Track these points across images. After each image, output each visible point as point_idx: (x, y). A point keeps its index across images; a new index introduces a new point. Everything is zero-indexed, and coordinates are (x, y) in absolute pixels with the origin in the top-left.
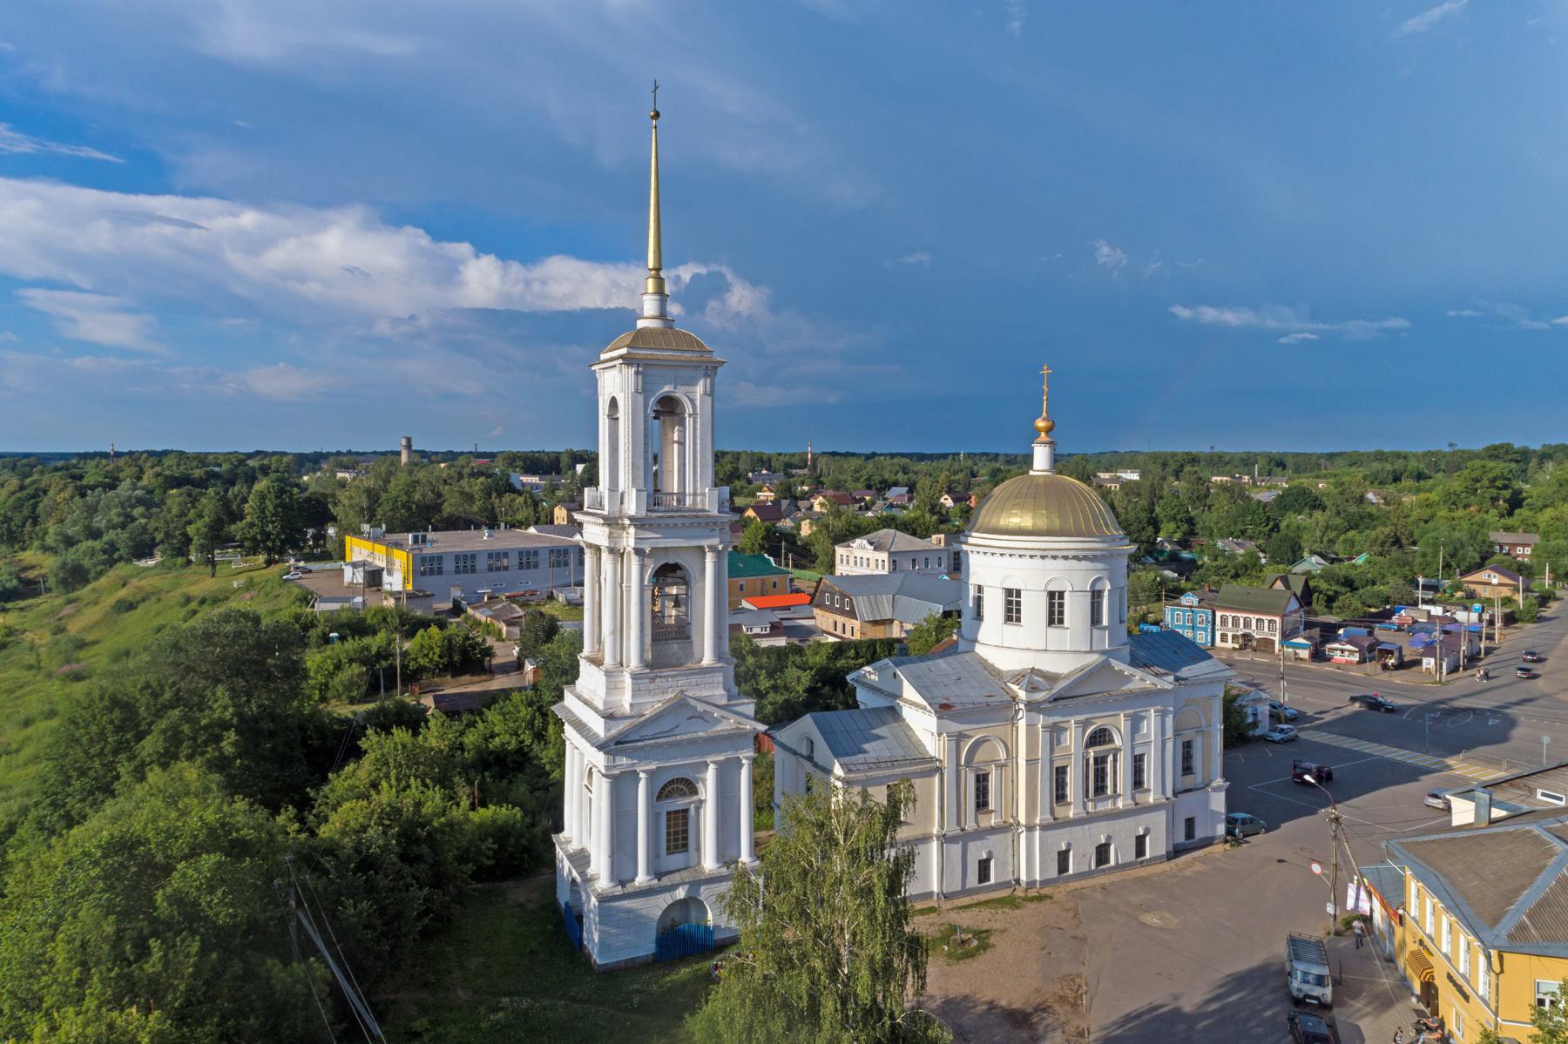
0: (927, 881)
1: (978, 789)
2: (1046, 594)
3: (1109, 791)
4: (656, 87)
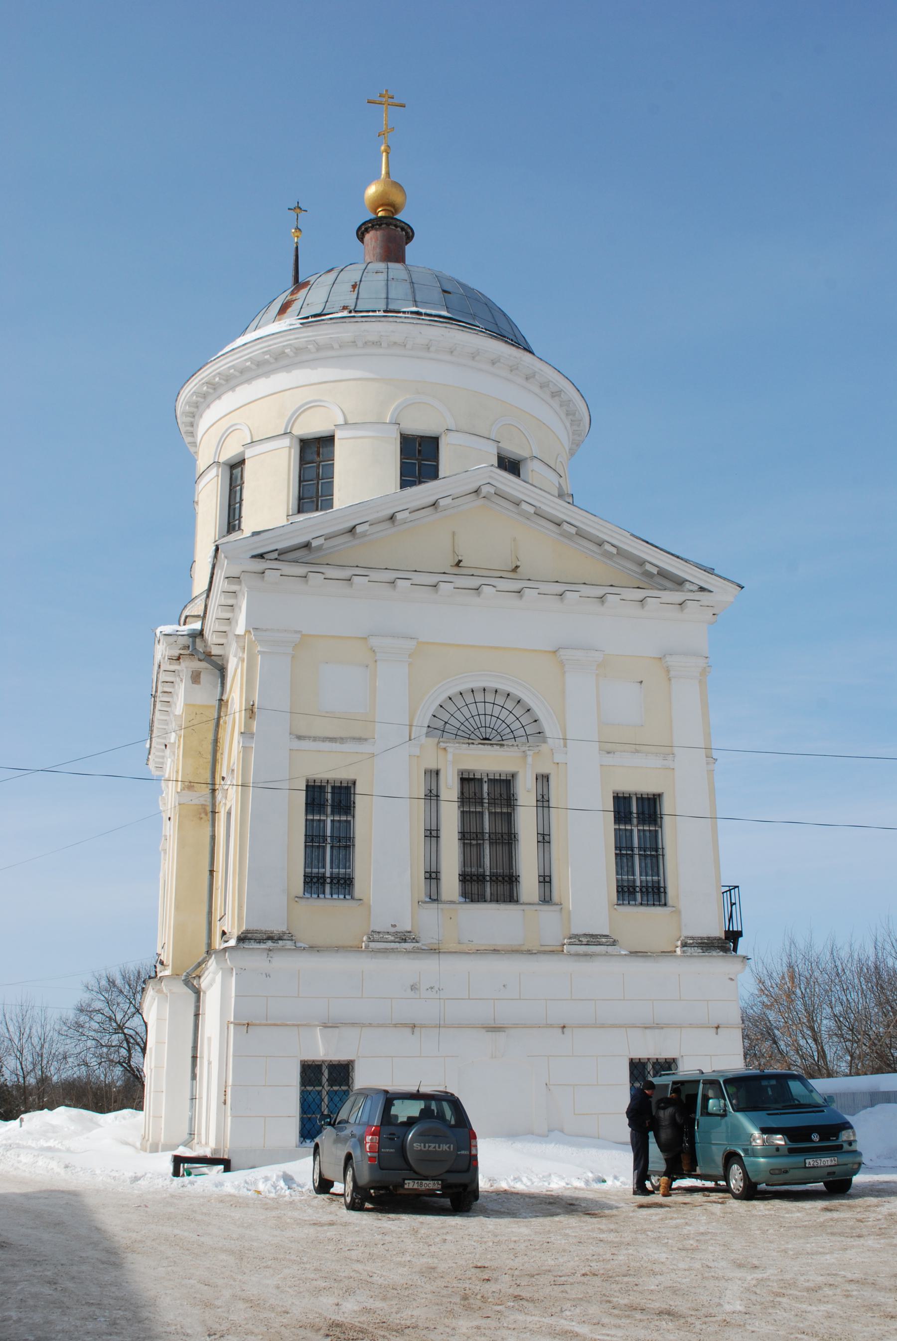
1: (545, 951)
2: (286, 442)
3: (529, 885)
4: (739, 586)
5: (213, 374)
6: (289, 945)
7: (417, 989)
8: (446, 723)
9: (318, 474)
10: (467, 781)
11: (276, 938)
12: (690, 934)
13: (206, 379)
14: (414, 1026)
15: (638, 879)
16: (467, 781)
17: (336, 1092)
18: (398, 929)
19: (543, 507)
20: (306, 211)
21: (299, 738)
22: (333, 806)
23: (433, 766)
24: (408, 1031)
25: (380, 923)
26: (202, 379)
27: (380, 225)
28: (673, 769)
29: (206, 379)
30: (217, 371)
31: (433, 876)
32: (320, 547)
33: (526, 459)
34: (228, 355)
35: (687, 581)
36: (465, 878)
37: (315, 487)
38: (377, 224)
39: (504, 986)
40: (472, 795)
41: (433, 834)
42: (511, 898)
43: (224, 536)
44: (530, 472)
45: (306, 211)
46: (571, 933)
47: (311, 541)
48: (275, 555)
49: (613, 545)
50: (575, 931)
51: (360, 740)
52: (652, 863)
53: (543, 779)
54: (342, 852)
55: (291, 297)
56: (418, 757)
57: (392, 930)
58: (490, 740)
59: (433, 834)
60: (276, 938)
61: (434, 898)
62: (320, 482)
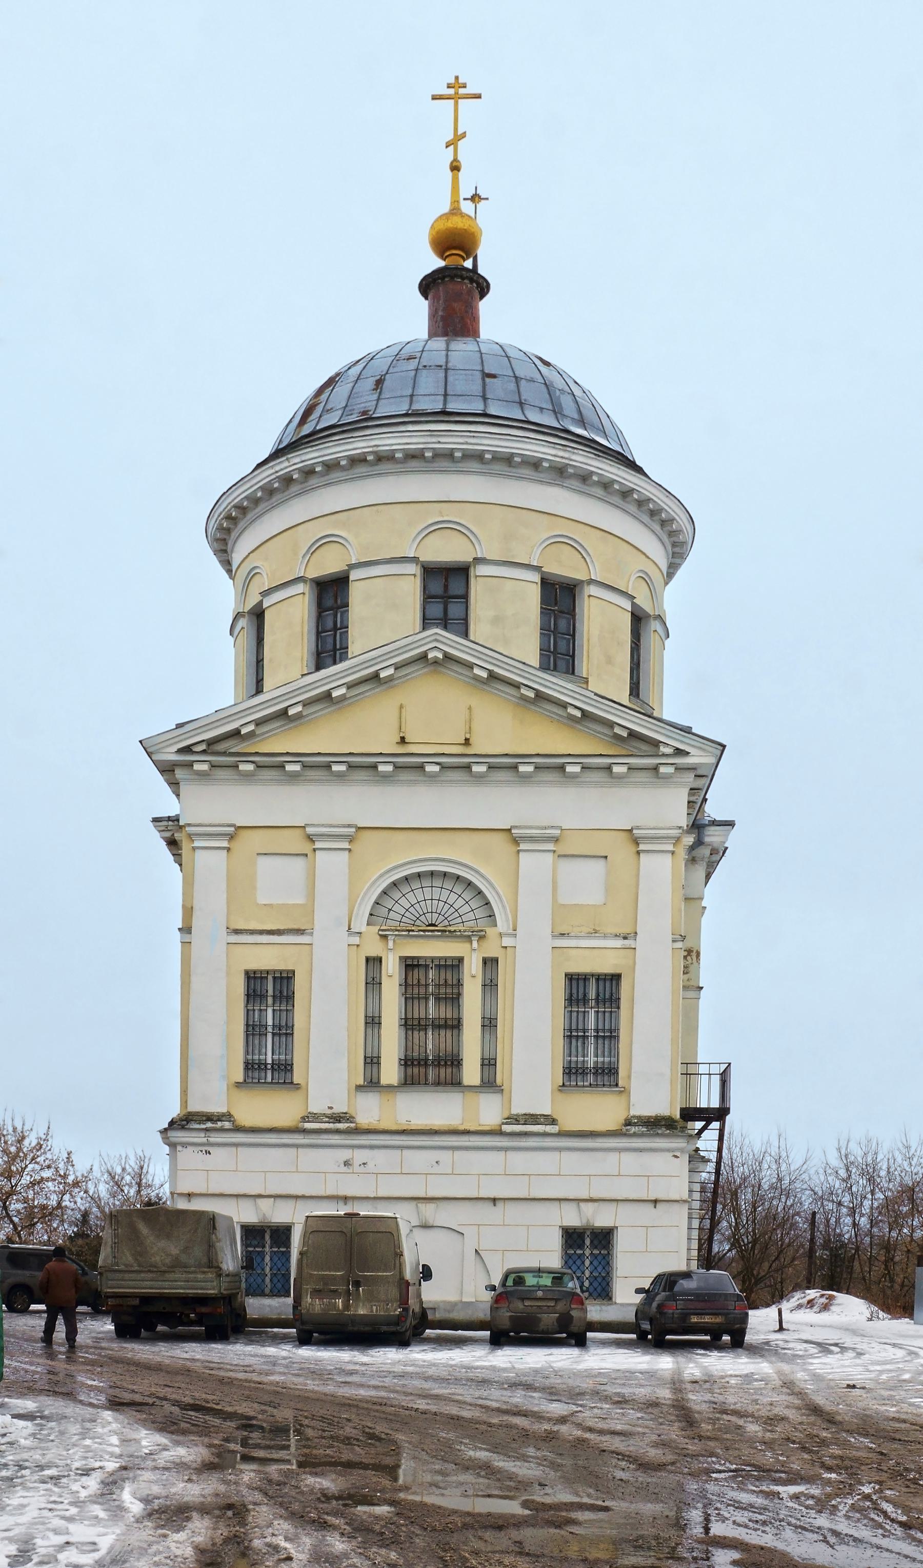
0: (293, 1333)
3: (471, 1073)
5: (229, 508)
6: (227, 1125)
7: (350, 1165)
8: (390, 910)
9: (335, 623)
10: (410, 965)
11: (215, 1119)
12: (637, 1113)
13: (223, 513)
14: (189, 1195)
15: (591, 1061)
16: (410, 965)
17: (275, 1252)
18: (334, 1111)
19: (497, 670)
20: (487, 199)
21: (237, 932)
22: (274, 997)
23: (373, 953)
24: (651, 1205)
25: (316, 1106)
26: (221, 514)
27: (443, 278)
28: (635, 948)
29: (223, 513)
30: (232, 504)
31: (372, 1061)
32: (251, 734)
33: (582, 581)
34: (239, 485)
35: (662, 742)
36: (407, 1062)
37: (332, 637)
38: (439, 278)
39: (437, 1162)
40: (415, 982)
41: (373, 1022)
42: (455, 1083)
43: (253, 696)
44: (586, 597)
45: (487, 199)
46: (632, 1113)
47: (240, 728)
48: (203, 747)
49: (576, 707)
50: (514, 1111)
51: (300, 932)
52: (596, 1048)
53: (490, 963)
54: (283, 1039)
55: (315, 400)
56: (358, 946)
57: (329, 1112)
58: (437, 926)
59: (373, 1022)
60: (215, 1119)
61: (372, 1084)
62: (338, 632)
